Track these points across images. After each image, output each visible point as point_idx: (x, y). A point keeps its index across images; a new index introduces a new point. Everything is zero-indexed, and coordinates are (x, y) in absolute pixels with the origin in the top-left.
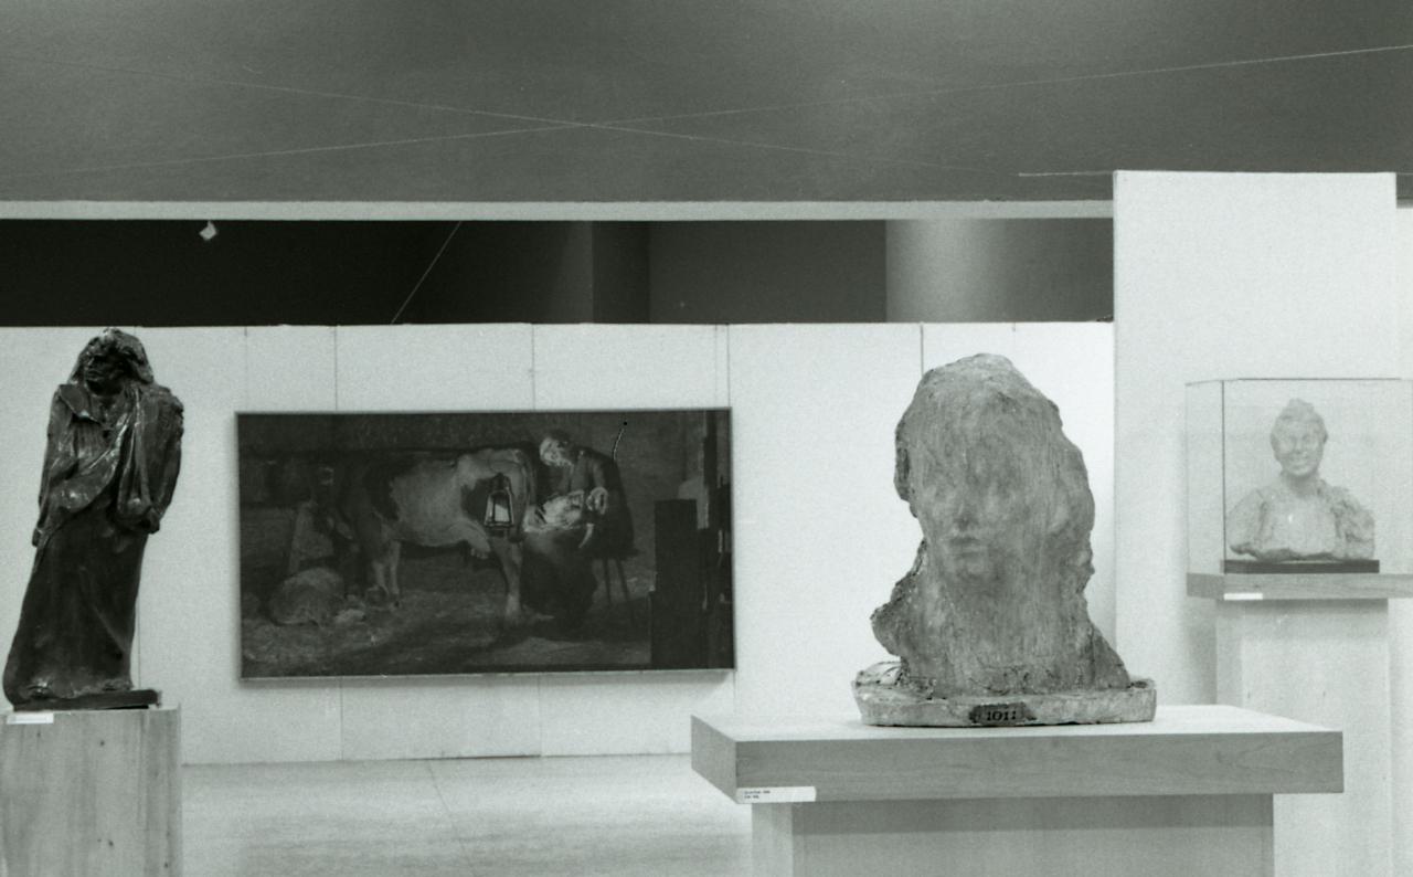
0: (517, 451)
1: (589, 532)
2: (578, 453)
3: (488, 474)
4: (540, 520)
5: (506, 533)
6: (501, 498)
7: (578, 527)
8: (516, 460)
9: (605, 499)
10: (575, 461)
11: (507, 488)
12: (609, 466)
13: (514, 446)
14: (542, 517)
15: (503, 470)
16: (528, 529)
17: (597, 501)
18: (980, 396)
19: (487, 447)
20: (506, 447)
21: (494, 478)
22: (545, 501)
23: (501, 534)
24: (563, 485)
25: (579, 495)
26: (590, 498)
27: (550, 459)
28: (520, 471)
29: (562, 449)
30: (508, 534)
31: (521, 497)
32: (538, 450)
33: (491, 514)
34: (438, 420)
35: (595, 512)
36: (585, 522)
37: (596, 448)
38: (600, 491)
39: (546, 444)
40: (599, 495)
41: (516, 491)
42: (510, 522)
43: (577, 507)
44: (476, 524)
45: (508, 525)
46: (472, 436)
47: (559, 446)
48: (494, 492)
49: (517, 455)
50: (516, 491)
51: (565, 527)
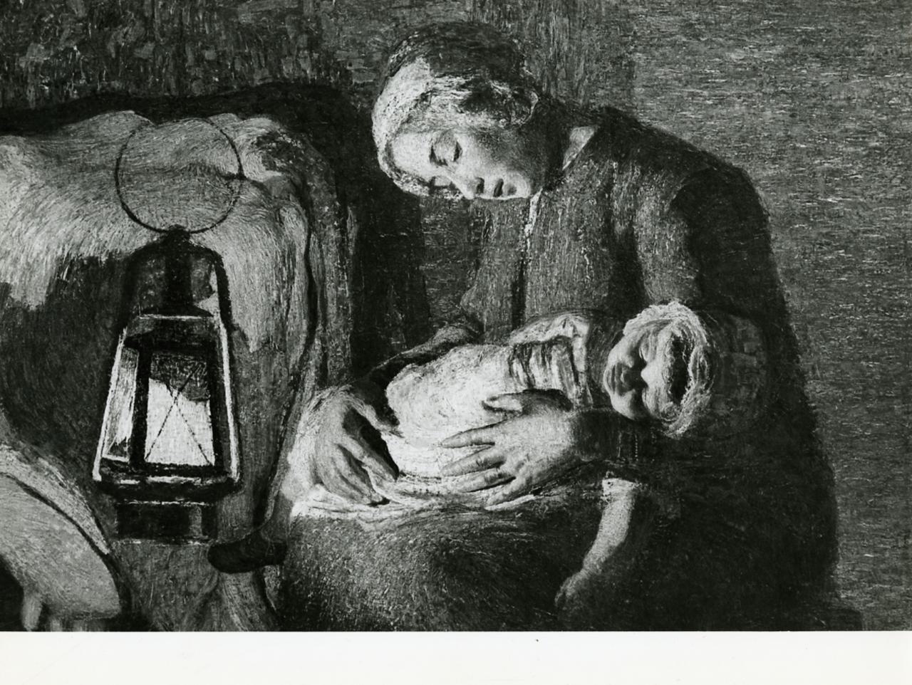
0: (261, 125)
1: (614, 524)
2: (560, 143)
3: (115, 236)
4: (372, 464)
5: (197, 522)
6: (179, 350)
7: (558, 495)
8: (255, 169)
9: (697, 353)
10: (549, 178)
11: (211, 304)
12: (715, 201)
13: (246, 102)
14: (378, 448)
15: (189, 212)
16: (305, 501)
17: (656, 374)
18: (523, 171)
19: (116, 102)
20: (202, 108)
21: (148, 251)
22: (391, 373)
23: (171, 528)
24: (486, 293)
25: (564, 342)
26: (618, 355)
27: (427, 170)
28: (276, 221)
29: (483, 119)
30: (210, 525)
31: (275, 343)
32: (365, 124)
33: (125, 430)
34: (532, 626)
35: (645, 422)
36: (596, 472)
37: (652, 113)
38: (665, 322)
39: (405, 86)
40: (664, 338)
41: (253, 324)
42: (220, 467)
43: (556, 399)
44: (49, 479)
45: (211, 483)
46: (38, 54)
47: (469, 105)
48: (145, 322)
49: (260, 143)
50: (252, 321)
51: (493, 499)
